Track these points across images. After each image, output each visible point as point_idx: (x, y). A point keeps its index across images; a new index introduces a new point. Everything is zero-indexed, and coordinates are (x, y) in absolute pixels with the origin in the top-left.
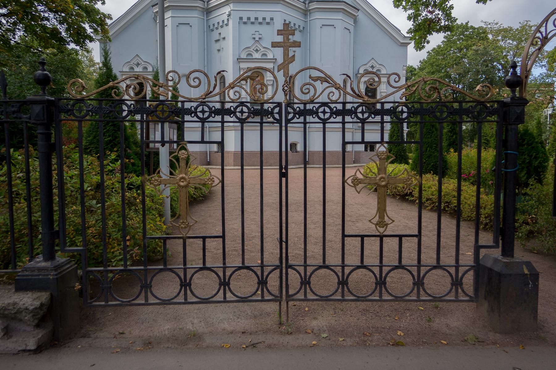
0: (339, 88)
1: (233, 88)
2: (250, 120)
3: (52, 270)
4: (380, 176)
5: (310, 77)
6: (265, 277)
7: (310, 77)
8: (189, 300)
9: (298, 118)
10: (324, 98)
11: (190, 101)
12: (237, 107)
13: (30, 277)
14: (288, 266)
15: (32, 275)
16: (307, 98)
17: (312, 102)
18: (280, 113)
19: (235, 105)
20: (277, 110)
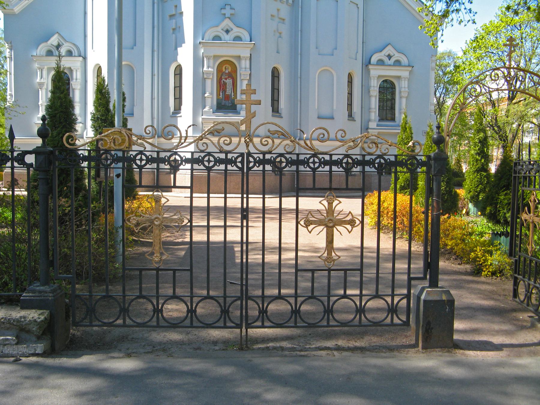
0: (294, 141)
1: (201, 140)
2: (341, 157)
3: (50, 292)
4: (329, 218)
5: (269, 131)
6: (223, 317)
7: (269, 131)
8: (161, 324)
9: (258, 167)
10: (281, 150)
11: (165, 151)
12: (205, 156)
13: (33, 298)
14: (248, 298)
15: (34, 296)
16: (265, 149)
17: (270, 152)
18: (249, 162)
19: (203, 155)
20: (239, 159)
